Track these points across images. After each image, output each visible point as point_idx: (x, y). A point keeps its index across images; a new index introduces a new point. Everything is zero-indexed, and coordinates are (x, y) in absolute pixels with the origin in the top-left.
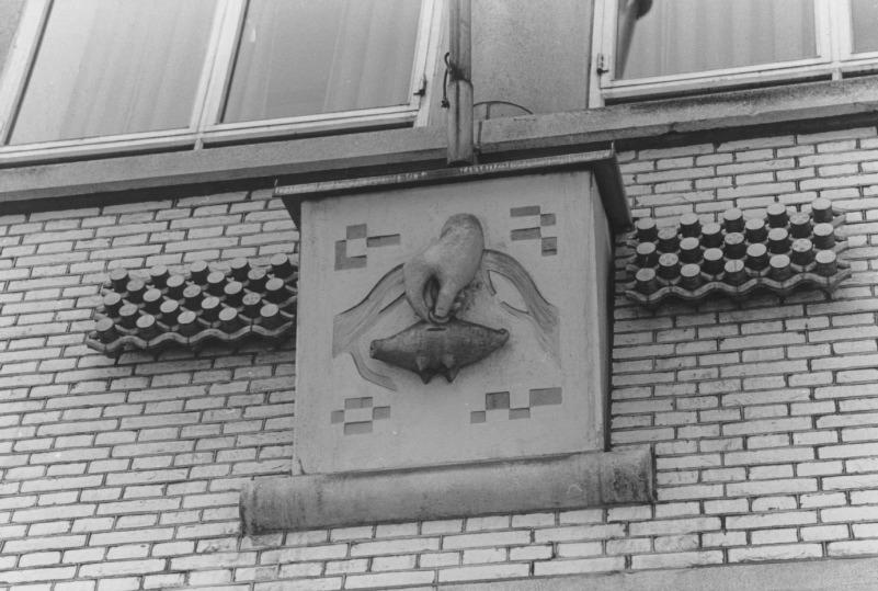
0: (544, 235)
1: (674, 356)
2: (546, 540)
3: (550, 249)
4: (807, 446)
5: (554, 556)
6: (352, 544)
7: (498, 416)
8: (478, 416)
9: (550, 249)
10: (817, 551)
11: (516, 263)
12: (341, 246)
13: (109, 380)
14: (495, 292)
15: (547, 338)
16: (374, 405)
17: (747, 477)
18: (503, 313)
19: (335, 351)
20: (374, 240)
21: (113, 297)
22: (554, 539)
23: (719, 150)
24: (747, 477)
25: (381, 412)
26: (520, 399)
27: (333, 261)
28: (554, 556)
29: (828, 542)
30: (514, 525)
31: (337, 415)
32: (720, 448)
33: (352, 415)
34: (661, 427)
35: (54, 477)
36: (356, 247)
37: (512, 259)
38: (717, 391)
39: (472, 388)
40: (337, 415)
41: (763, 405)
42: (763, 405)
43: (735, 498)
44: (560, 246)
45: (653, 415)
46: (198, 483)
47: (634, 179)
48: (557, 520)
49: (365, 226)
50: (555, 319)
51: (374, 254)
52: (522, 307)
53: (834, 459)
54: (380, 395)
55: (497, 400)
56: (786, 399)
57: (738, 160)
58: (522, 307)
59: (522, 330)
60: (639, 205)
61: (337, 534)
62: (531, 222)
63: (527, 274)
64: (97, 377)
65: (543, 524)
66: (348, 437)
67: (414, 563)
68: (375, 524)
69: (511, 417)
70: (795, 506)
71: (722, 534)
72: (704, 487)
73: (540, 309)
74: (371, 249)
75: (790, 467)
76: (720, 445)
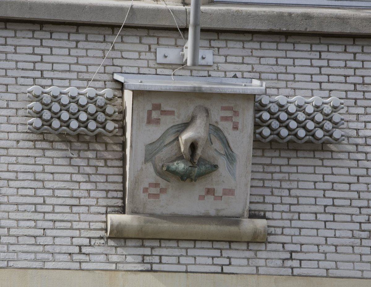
0: (234, 120)
1: (271, 165)
2: (226, 256)
3: (236, 128)
4: (322, 221)
5: (230, 264)
6: (152, 248)
7: (210, 198)
8: (201, 198)
9: (236, 128)
10: (324, 273)
11: (222, 132)
12: (150, 113)
13: (34, 141)
14: (212, 144)
15: (231, 167)
16: (161, 188)
17: (300, 233)
18: (215, 154)
19: (146, 161)
20: (164, 113)
21: (37, 106)
22: (230, 256)
23: (288, 41)
24: (300, 233)
25: (163, 191)
26: (219, 193)
27: (145, 120)
28: (230, 264)
29: (328, 269)
30: (214, 247)
31: (145, 190)
32: (290, 217)
33: (153, 191)
34: (267, 203)
35: (22, 196)
36: (155, 115)
37: (221, 131)
38: (288, 187)
39: (199, 188)
40: (145, 190)
41: (306, 197)
42: (306, 197)
43: (296, 244)
44: (240, 127)
45: (264, 196)
46: (84, 207)
47: (252, 52)
48: (230, 246)
49: (160, 105)
50: (235, 159)
51: (163, 118)
52: (222, 152)
53: (332, 229)
54: (163, 183)
55: (210, 191)
56: (315, 195)
57: (296, 49)
58: (222, 152)
59: (222, 162)
60: (254, 70)
61: (147, 243)
62: (228, 114)
63: (225, 137)
64: (28, 138)
65: (225, 247)
66: (149, 200)
67: (178, 261)
68: (160, 240)
69: (215, 199)
70: (317, 250)
71: (290, 261)
72: (284, 236)
73: (230, 157)
74: (162, 116)
75: (316, 230)
76: (289, 216)
